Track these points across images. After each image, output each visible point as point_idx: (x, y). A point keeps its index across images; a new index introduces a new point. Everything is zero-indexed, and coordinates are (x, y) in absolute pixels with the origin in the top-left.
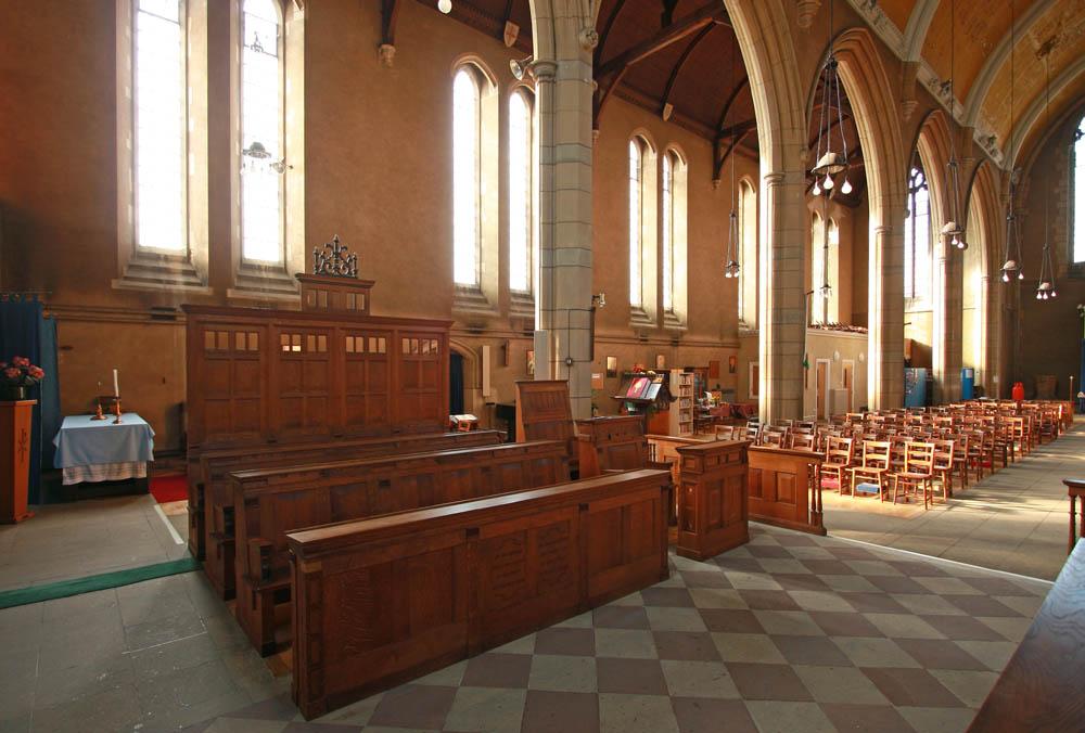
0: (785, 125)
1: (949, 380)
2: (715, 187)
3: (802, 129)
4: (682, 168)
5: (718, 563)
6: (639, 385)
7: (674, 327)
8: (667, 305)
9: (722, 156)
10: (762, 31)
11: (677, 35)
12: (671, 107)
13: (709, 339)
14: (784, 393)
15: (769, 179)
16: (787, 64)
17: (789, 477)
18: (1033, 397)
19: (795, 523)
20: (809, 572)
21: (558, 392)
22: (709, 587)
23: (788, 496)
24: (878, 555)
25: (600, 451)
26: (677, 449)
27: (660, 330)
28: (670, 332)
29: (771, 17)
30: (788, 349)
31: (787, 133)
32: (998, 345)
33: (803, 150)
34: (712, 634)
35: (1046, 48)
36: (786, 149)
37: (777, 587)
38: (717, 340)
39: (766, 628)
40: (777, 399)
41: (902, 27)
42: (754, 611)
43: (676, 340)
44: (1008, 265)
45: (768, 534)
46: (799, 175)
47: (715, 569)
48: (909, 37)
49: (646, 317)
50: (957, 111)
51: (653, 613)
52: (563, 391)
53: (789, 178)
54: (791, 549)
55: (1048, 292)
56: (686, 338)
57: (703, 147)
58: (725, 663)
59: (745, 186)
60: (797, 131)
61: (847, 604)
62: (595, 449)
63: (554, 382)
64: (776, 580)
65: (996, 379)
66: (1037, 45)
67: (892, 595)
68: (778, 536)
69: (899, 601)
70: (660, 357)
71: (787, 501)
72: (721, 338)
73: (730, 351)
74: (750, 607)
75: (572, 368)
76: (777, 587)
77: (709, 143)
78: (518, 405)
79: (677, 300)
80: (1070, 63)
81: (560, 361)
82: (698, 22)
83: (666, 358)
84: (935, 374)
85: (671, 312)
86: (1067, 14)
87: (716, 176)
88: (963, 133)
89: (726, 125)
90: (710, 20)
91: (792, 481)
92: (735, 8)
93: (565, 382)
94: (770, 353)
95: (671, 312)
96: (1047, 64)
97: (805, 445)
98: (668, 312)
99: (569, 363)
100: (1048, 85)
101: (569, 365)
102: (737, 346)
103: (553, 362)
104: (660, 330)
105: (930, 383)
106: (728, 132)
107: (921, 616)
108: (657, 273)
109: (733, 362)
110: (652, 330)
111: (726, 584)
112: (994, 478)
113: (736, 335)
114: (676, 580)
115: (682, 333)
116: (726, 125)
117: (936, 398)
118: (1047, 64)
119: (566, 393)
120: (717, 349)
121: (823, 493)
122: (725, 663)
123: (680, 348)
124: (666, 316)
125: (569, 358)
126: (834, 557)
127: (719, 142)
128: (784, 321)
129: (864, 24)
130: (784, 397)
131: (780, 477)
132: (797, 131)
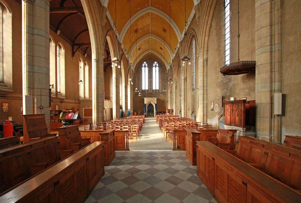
0: (99, 48)
1: (126, 112)
2: (73, 59)
3: (103, 50)
4: (63, 51)
5: (114, 164)
6: (70, 115)
7: (61, 97)
8: (58, 90)
9: (75, 51)
10: (94, 21)
11: (66, 11)
12: (60, 32)
13: (71, 101)
14: (99, 116)
15: (95, 60)
16: (100, 32)
17: (120, 137)
18: (137, 115)
19: (122, 149)
20: (134, 160)
21: (41, 118)
22: (117, 173)
23: (120, 142)
24: (143, 152)
25: (68, 138)
26: (100, 134)
27: (57, 98)
28: (60, 99)
29: (96, 19)
30: (100, 104)
31: (99, 50)
32: (132, 104)
33: (103, 55)
34: (130, 186)
35: (139, 49)
36: (99, 54)
37: (132, 167)
38: (74, 101)
39: (119, 179)
40: (98, 118)
41: (119, 34)
42: (133, 175)
43: (62, 101)
44: (136, 89)
45: (118, 153)
46: (102, 61)
47: (113, 167)
48: (120, 37)
49: (61, 95)
50: (127, 56)
51: (110, 187)
52: (43, 118)
53: (100, 61)
54: (126, 155)
55: (140, 95)
56: (65, 100)
57: (70, 47)
58: (141, 193)
59: (80, 61)
60: (102, 50)
61: (148, 166)
62: (66, 137)
63: (34, 115)
64: (130, 165)
65: (132, 111)
66: (138, 48)
67: (153, 161)
68: (120, 153)
69: (156, 162)
70: (57, 106)
71: (120, 144)
72: (75, 101)
73: (77, 105)
74: (131, 174)
75: (42, 110)
76: (132, 167)
77: (71, 46)
78: (24, 124)
79: (147, 88)
80: (143, 52)
81: (37, 107)
82: (73, 11)
83: (59, 106)
84: (123, 110)
85: (60, 92)
86: (142, 44)
87: (73, 55)
88: (128, 61)
89: (76, 42)
90: (76, 12)
91: (121, 138)
92: (87, 12)
93: (44, 114)
94: (96, 105)
95: (60, 92)
96: (139, 52)
97: (101, 129)
98: (59, 93)
99: (41, 108)
100: (140, 55)
101: (41, 109)
102: (79, 103)
103: (34, 107)
104: (57, 98)
105: (122, 112)
106: (77, 45)
107: (162, 164)
108: (58, 81)
109: (78, 108)
110: (54, 97)
111: (120, 170)
112: (142, 131)
113: (79, 100)
114: (107, 174)
115: (63, 99)
116: (76, 42)
117: (123, 116)
118: (139, 52)
119: (44, 118)
120: (74, 104)
121: (129, 140)
122: (141, 193)
123: (63, 104)
124: (58, 94)
125: (43, 107)
126: (136, 155)
127: (77, 48)
128: (99, 97)
129: (113, 31)
130: (99, 117)
131: (118, 137)
132: (102, 50)
